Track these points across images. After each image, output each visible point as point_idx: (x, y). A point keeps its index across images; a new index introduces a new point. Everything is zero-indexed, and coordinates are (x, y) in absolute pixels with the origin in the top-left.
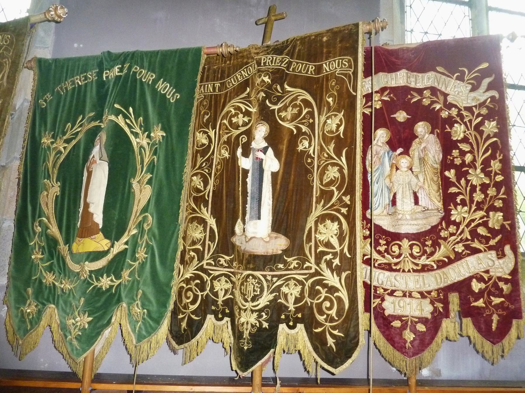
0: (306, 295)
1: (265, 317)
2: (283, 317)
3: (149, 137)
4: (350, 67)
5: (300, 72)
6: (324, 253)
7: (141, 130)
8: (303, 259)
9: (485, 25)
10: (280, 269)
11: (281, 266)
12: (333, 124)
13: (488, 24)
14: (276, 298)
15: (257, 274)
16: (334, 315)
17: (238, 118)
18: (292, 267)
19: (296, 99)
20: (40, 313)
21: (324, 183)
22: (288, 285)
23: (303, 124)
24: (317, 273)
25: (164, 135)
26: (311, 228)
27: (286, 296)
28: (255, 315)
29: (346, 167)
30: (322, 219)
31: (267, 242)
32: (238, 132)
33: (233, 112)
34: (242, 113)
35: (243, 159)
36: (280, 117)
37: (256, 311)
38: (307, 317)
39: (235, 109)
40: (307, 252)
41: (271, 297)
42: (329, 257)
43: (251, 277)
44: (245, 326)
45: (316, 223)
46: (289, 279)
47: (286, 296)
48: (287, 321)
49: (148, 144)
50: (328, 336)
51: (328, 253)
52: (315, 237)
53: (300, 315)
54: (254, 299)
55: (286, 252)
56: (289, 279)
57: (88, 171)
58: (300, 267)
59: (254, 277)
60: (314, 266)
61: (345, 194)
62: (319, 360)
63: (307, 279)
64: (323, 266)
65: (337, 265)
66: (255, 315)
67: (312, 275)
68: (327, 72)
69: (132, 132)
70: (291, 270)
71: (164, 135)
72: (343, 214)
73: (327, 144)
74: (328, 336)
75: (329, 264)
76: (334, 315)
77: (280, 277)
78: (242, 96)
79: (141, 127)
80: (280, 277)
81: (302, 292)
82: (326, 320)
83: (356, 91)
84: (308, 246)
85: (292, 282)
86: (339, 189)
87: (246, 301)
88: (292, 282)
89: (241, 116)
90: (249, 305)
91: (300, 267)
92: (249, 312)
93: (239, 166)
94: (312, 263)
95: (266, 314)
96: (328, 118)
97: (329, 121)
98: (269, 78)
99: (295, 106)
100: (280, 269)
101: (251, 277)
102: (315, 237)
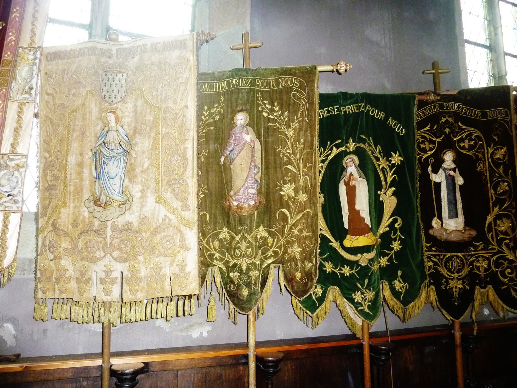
0: (493, 266)
1: (467, 282)
2: (477, 281)
3: (387, 160)
4: (507, 115)
5: (471, 115)
6: (503, 239)
7: (380, 155)
8: (487, 243)
9: (504, 66)
10: (472, 251)
11: (472, 249)
12: (500, 154)
13: (505, 65)
14: (472, 269)
15: (460, 255)
16: (514, 277)
17: (425, 144)
18: (480, 249)
19: (471, 134)
20: (324, 293)
21: (498, 193)
22: (478, 261)
23: (479, 152)
24: (499, 252)
25: (402, 159)
26: (491, 223)
27: (478, 268)
28: (461, 281)
29: (511, 183)
30: (498, 217)
31: (463, 233)
32: (425, 156)
33: (421, 140)
34: (427, 141)
35: (434, 175)
36: (459, 146)
37: (461, 279)
38: (492, 279)
39: (421, 138)
40: (490, 239)
41: (469, 269)
42: (508, 241)
43: (455, 257)
44: (454, 289)
45: (495, 220)
46: (479, 257)
47: (478, 268)
48: (479, 284)
49: (389, 166)
50: (512, 291)
51: (506, 239)
52: (495, 229)
53: (488, 279)
54: (459, 271)
55: (476, 239)
56: (479, 257)
57: (347, 184)
58: (485, 248)
59: (458, 257)
60: (497, 248)
61: (513, 201)
62: (505, 306)
63: (492, 256)
64: (504, 247)
65: (512, 246)
66: (461, 281)
67: (494, 254)
68: (490, 117)
69: (374, 156)
70: (479, 251)
71: (402, 159)
72: (512, 213)
73: (498, 167)
74: (512, 291)
75: (507, 245)
76: (514, 277)
77: (472, 256)
78: (426, 129)
79: (380, 153)
80: (472, 256)
81: (489, 265)
82: (509, 281)
83: (512, 133)
84: (490, 235)
85: (481, 259)
86: (509, 197)
87: (453, 273)
88: (481, 259)
89: (427, 143)
90: (455, 275)
91: (485, 248)
92: (455, 280)
93: (431, 180)
94: (494, 245)
95: (467, 280)
96: (495, 150)
97: (497, 152)
98: (452, 119)
99: (470, 140)
100: (472, 251)
101: (455, 257)
102: (495, 229)
